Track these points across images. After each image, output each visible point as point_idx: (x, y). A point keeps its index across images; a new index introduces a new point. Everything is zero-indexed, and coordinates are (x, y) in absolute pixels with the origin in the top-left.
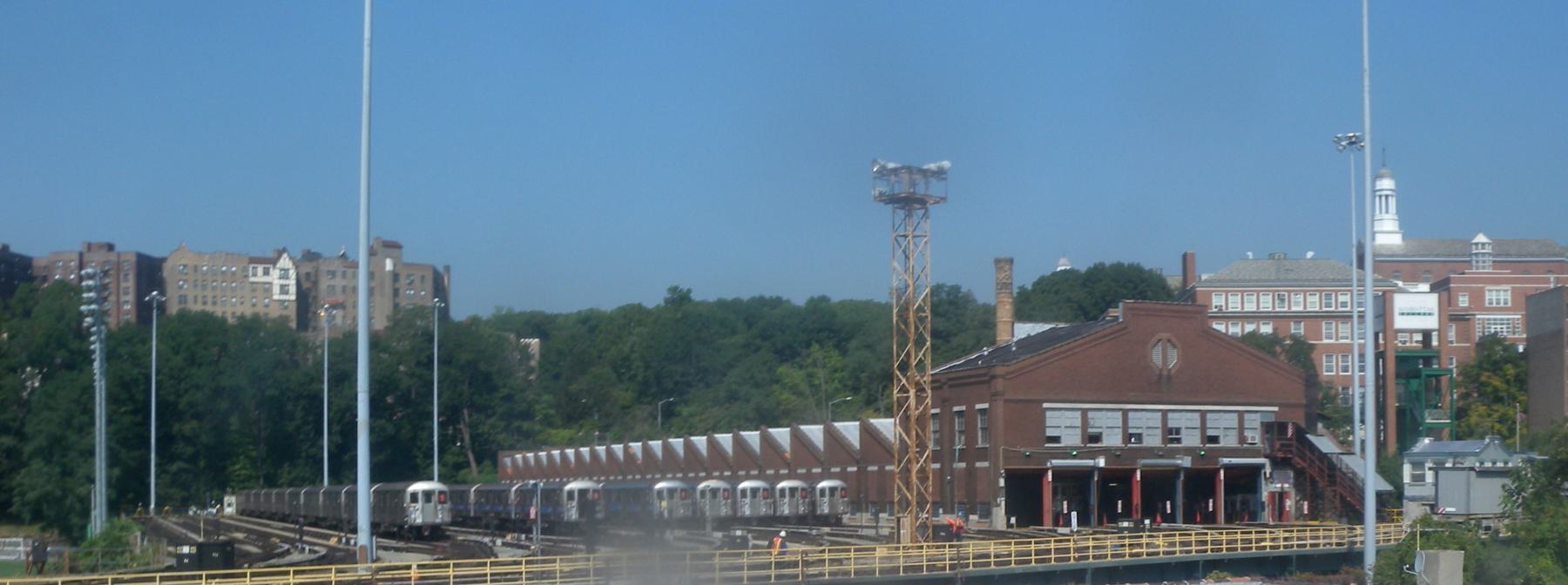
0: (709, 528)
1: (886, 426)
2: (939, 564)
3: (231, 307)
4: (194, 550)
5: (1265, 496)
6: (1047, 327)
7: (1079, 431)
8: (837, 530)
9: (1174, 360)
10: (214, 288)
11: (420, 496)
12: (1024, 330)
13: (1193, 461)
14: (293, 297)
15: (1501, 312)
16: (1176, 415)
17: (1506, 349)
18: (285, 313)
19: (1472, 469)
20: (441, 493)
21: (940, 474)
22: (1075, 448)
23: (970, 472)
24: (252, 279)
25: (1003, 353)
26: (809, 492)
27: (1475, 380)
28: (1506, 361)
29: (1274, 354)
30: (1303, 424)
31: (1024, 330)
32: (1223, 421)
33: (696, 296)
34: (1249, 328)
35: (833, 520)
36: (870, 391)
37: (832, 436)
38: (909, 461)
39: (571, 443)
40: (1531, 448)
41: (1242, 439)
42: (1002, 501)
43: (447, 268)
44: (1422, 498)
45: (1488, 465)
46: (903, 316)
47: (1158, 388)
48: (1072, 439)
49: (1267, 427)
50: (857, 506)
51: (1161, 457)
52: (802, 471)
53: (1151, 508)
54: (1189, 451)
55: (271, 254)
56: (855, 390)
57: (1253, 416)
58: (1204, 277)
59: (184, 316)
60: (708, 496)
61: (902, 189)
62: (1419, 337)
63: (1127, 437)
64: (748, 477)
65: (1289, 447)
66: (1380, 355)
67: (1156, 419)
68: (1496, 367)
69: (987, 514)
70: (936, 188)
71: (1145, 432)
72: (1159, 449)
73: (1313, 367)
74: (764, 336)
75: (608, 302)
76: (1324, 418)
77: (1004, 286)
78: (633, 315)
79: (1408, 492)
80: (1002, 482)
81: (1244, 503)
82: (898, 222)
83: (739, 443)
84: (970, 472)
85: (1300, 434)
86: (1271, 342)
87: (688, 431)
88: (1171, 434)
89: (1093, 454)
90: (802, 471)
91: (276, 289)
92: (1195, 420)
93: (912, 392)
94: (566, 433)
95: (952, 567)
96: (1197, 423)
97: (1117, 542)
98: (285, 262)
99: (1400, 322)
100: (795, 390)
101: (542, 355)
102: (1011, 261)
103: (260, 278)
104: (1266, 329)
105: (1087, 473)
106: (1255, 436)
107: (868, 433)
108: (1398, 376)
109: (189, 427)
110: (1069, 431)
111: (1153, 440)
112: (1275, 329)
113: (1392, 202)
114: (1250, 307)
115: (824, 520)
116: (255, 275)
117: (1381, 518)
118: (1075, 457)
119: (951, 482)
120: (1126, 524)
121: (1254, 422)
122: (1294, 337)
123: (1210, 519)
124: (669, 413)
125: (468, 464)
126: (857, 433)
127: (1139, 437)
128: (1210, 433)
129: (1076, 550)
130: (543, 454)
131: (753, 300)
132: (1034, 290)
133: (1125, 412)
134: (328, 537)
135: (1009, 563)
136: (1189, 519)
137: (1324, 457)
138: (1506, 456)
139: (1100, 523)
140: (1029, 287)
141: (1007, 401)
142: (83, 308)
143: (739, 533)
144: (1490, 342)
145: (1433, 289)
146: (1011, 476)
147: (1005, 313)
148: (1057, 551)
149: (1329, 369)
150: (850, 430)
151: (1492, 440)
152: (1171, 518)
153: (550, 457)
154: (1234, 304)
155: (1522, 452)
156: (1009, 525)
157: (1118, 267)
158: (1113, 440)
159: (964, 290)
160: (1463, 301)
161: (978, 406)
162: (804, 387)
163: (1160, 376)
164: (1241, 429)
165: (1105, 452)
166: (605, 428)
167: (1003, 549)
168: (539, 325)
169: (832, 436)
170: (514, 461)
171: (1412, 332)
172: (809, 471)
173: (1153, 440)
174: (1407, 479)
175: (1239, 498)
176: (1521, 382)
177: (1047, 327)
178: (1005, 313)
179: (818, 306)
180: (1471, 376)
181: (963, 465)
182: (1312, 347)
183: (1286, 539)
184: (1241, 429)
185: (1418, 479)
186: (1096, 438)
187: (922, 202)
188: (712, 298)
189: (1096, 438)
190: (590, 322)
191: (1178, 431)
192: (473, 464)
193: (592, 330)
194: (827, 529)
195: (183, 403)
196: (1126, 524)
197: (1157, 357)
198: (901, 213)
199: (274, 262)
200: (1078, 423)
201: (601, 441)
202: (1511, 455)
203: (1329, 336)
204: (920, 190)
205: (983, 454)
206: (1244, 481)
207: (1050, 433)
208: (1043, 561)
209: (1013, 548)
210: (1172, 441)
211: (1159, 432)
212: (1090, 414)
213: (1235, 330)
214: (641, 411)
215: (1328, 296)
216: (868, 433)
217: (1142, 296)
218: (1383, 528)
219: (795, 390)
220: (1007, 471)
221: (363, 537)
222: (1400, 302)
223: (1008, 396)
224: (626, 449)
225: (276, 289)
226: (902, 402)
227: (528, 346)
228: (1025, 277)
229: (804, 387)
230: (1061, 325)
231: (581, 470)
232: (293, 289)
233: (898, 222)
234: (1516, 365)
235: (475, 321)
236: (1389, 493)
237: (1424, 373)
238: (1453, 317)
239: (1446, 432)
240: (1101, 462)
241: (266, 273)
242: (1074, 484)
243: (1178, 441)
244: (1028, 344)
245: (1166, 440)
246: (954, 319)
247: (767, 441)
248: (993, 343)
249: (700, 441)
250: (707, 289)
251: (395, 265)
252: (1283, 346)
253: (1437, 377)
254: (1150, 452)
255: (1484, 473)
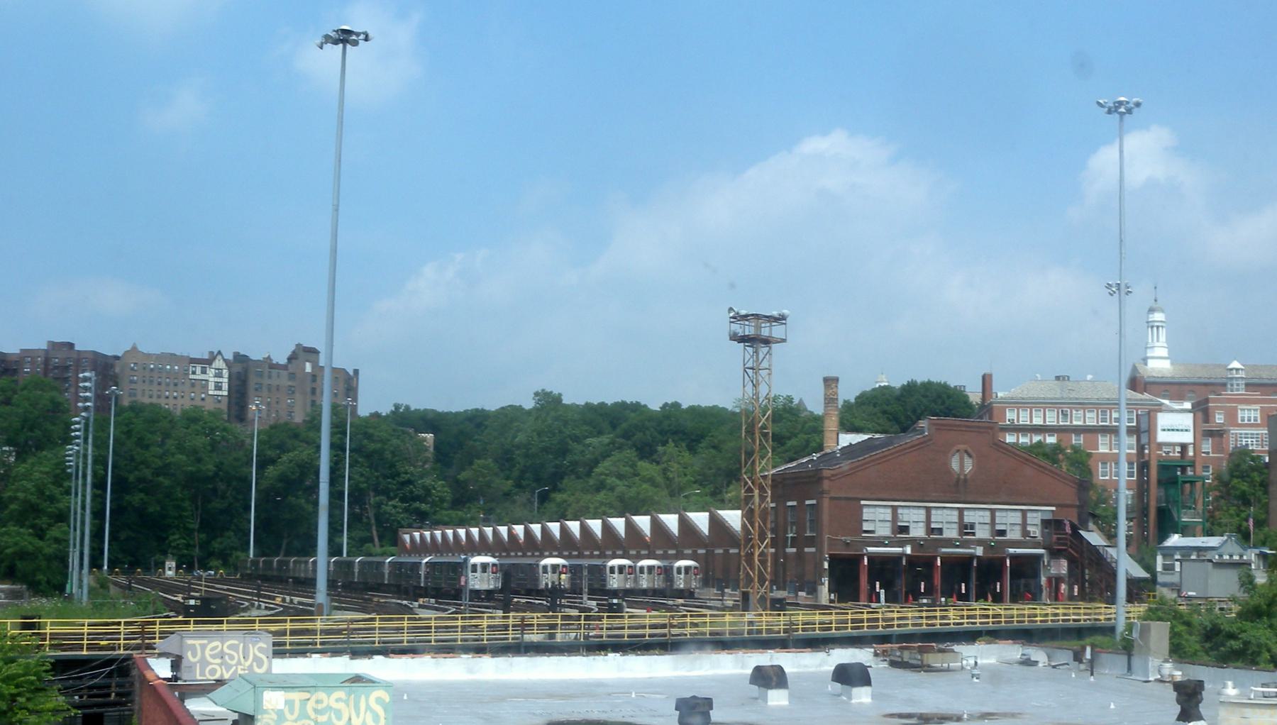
0: (585, 597)
1: (733, 518)
2: (776, 628)
3: (176, 402)
4: (199, 603)
5: (1043, 580)
6: (866, 437)
7: (889, 524)
8: (690, 602)
9: (969, 466)
10: (159, 384)
11: (549, 569)
12: (847, 439)
13: (984, 552)
14: (226, 393)
15: (1249, 430)
16: (972, 513)
17: (1253, 459)
18: (218, 406)
19: (1210, 561)
20: (494, 565)
21: (775, 556)
22: (886, 538)
23: (800, 556)
24: (192, 377)
25: (830, 458)
26: (667, 572)
27: (1226, 484)
28: (1253, 469)
29: (1055, 461)
30: (1076, 522)
31: (847, 439)
32: (1009, 518)
33: (566, 400)
34: (1036, 438)
35: (687, 594)
36: (716, 488)
37: (685, 524)
38: (753, 547)
39: (462, 523)
40: (1264, 544)
41: (1025, 533)
42: (826, 580)
43: (356, 372)
44: (1172, 584)
45: (1226, 557)
46: (750, 432)
47: (958, 490)
48: (884, 531)
49: (1046, 523)
50: (706, 582)
51: (957, 547)
52: (659, 552)
53: (950, 591)
54: (980, 542)
55: (206, 357)
56: (701, 484)
57: (1035, 515)
58: (1000, 395)
59: (136, 409)
60: (479, 569)
61: (749, 330)
62: (1178, 449)
63: (931, 531)
64: (614, 557)
65: (1064, 539)
66: (1144, 466)
67: (954, 516)
68: (1243, 476)
69: (813, 590)
70: (777, 331)
71: (945, 526)
72: (957, 540)
73: (1090, 472)
74: (627, 435)
75: (492, 403)
76: (1094, 516)
77: (830, 400)
78: (511, 415)
79: (1160, 579)
80: (826, 565)
81: (1026, 586)
82: (748, 357)
83: (607, 528)
84: (800, 556)
85: (1075, 529)
86: (1052, 454)
87: (561, 517)
88: (966, 528)
89: (902, 543)
90: (659, 552)
91: (211, 386)
92: (986, 517)
93: (756, 492)
94: (456, 514)
95: (785, 631)
96: (988, 520)
97: (917, 614)
98: (219, 363)
99: (1162, 437)
100: (651, 481)
101: (436, 448)
102: (836, 380)
103: (199, 376)
104: (1051, 440)
105: (896, 559)
106: (1035, 531)
107: (716, 523)
108: (1160, 482)
109: (136, 498)
110: (882, 524)
111: (951, 533)
112: (1059, 441)
113: (1163, 333)
114: (1038, 421)
115: (681, 594)
116: (194, 373)
117: (1131, 598)
118: (886, 546)
119: (784, 564)
120: (925, 601)
121: (1035, 519)
122: (1073, 447)
123: (998, 599)
124: (544, 498)
125: (371, 540)
126: (707, 522)
127: (940, 531)
128: (998, 527)
129: (884, 620)
130: (438, 533)
131: (616, 404)
132: (856, 402)
133: (928, 510)
134: (274, 598)
135: (830, 629)
136: (981, 596)
137: (1094, 550)
138: (1241, 551)
139: (907, 601)
140: (853, 401)
141: (831, 498)
142: (80, 404)
143: (615, 601)
144: (1243, 452)
145: (1193, 410)
146: (834, 560)
147: (832, 424)
148: (869, 620)
149: (1102, 475)
150: (701, 520)
151: (1229, 537)
152: (964, 598)
153: (444, 536)
154: (1024, 419)
155: (1255, 547)
156: (831, 601)
157: (928, 385)
158: (918, 532)
159: (796, 401)
160: (1219, 418)
161: (808, 502)
162: (660, 479)
163: (958, 479)
164: (1024, 524)
165: (913, 541)
166: (489, 511)
167: (826, 618)
168: (431, 421)
169: (685, 524)
170: (412, 538)
171: (1174, 445)
172: (666, 552)
173: (951, 533)
174: (1159, 568)
175: (1023, 581)
176: (1264, 486)
177: (866, 437)
178: (832, 424)
179: (672, 410)
180: (1224, 486)
181: (794, 550)
182: (1090, 455)
183: (1065, 615)
184: (1024, 524)
185: (1168, 568)
186: (905, 529)
187: (767, 342)
188: (581, 402)
189: (905, 529)
190: (477, 419)
191: (972, 526)
192: (376, 540)
193: (479, 425)
194: (681, 601)
195: (132, 478)
196: (925, 601)
197: (955, 465)
198: (750, 350)
199: (209, 362)
200: (889, 517)
201: (487, 522)
202: (1245, 549)
203: (1103, 446)
204: (765, 332)
205: (811, 542)
206: (1025, 569)
207: (866, 527)
208: (858, 628)
209: (833, 617)
210: (967, 534)
211: (956, 526)
212: (900, 511)
213: (1024, 440)
214: (521, 498)
215: (1104, 412)
216: (716, 523)
217: (948, 412)
218: (1130, 607)
219: (651, 481)
220: (831, 555)
221: (321, 595)
222: (1163, 420)
223: (833, 495)
224: (510, 531)
225: (211, 386)
226: (748, 499)
227: (425, 440)
228: (848, 392)
229: (660, 479)
230: (877, 436)
231: (482, 546)
232: (225, 386)
233: (748, 357)
234: (1261, 473)
235: (376, 415)
236: (1144, 580)
237: (1180, 480)
238: (1208, 431)
239: (1199, 528)
240: (908, 550)
241: (204, 372)
242: (885, 569)
243: (973, 534)
244: (850, 450)
245: (961, 533)
246: (791, 428)
247: (630, 526)
248: (820, 448)
249: (574, 526)
250: (576, 394)
251: (313, 368)
252: (1065, 454)
253: (1192, 483)
254: (949, 543)
255: (1221, 565)
